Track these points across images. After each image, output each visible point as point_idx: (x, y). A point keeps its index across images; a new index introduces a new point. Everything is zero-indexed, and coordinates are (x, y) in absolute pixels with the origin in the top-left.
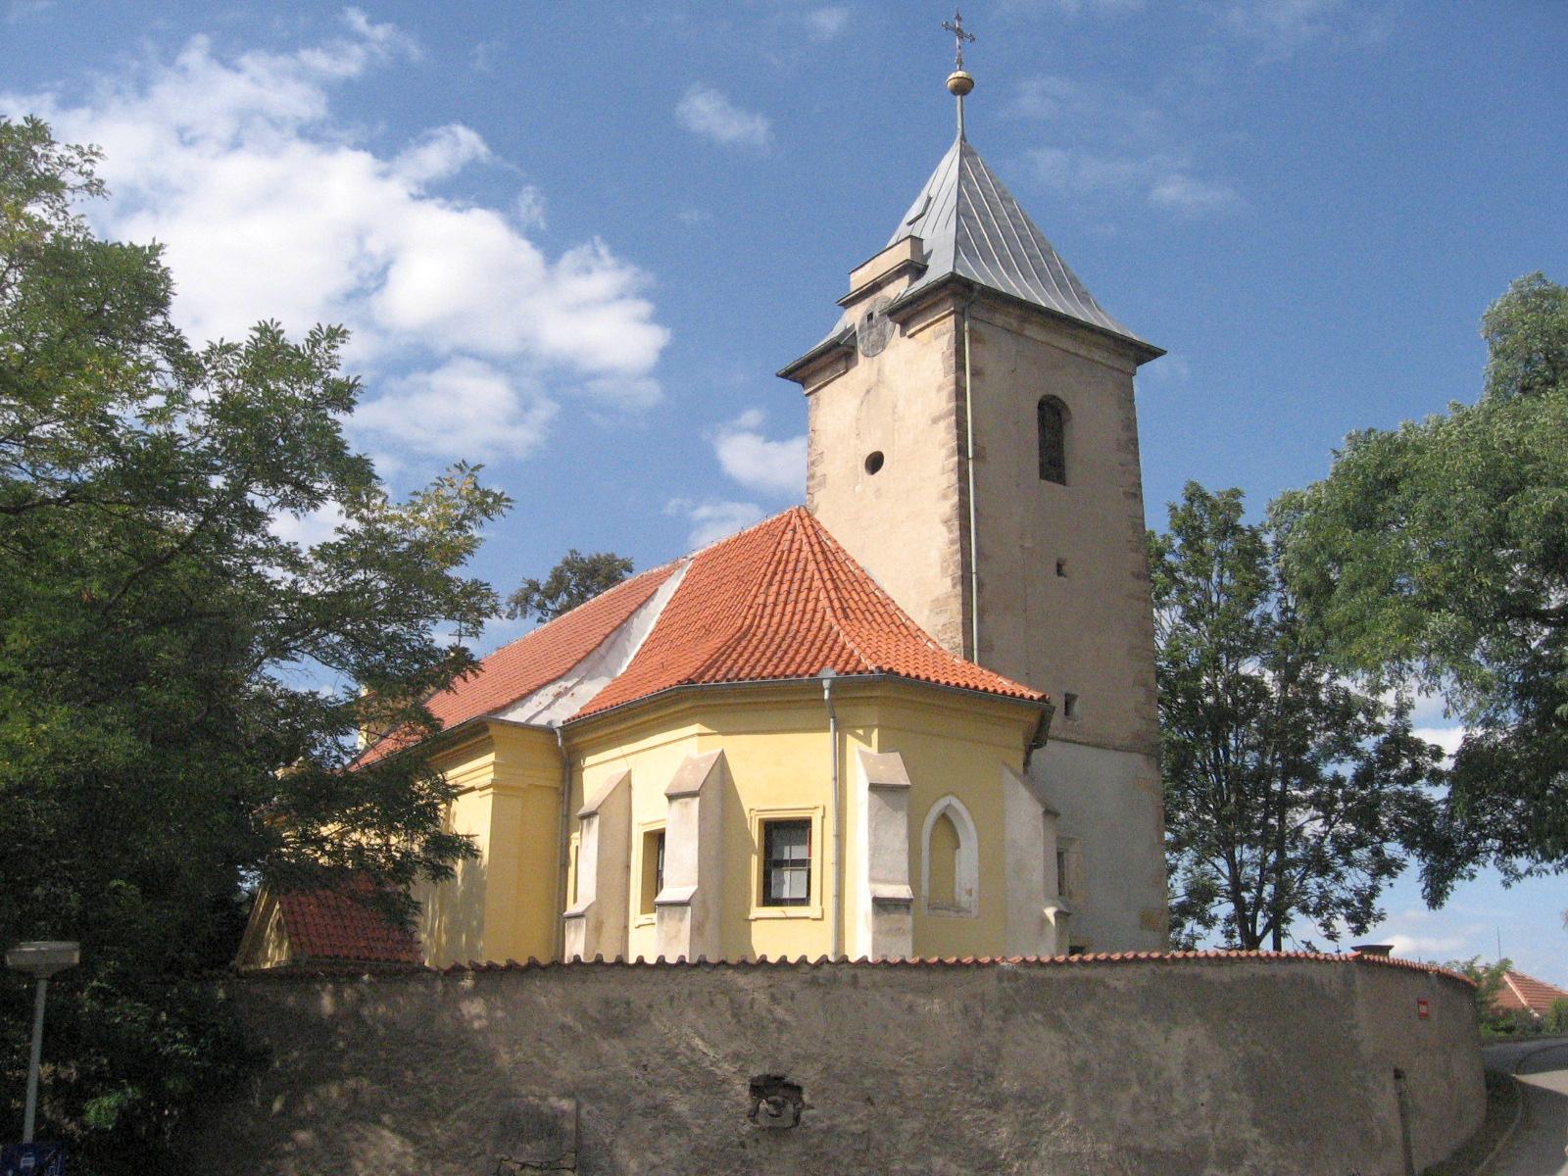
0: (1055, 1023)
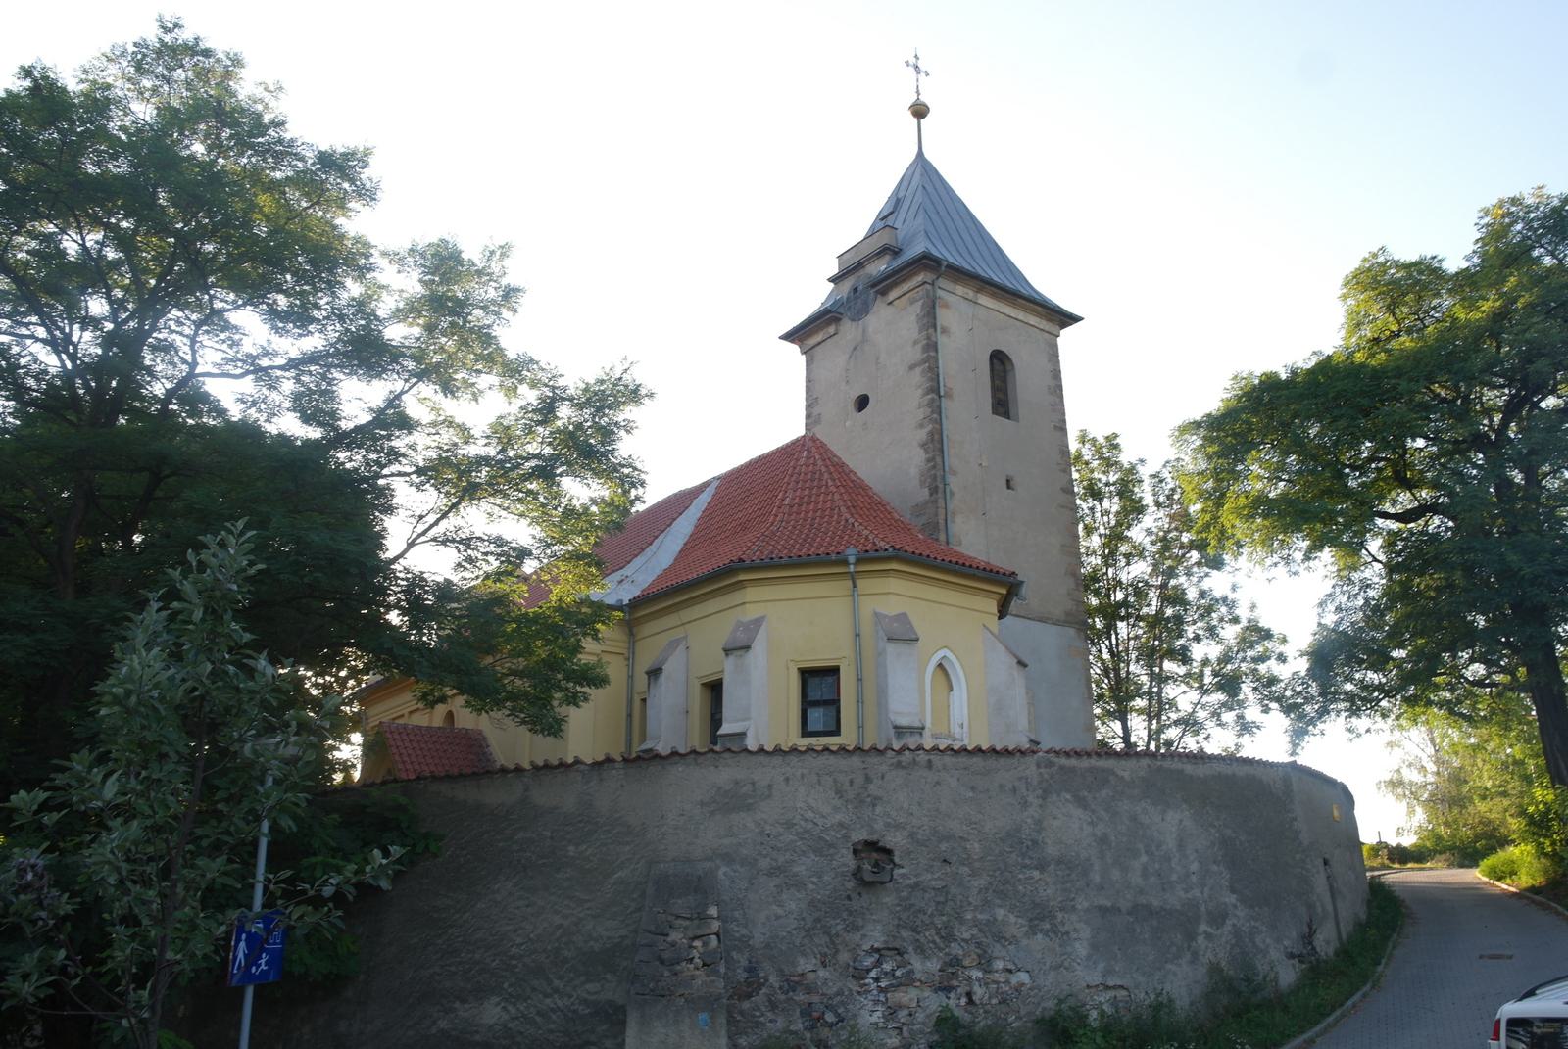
0: (1081, 803)
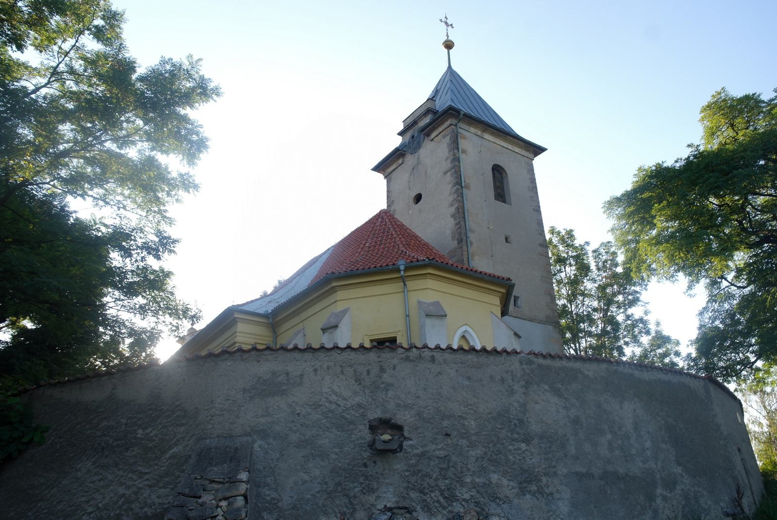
0: (558, 393)
